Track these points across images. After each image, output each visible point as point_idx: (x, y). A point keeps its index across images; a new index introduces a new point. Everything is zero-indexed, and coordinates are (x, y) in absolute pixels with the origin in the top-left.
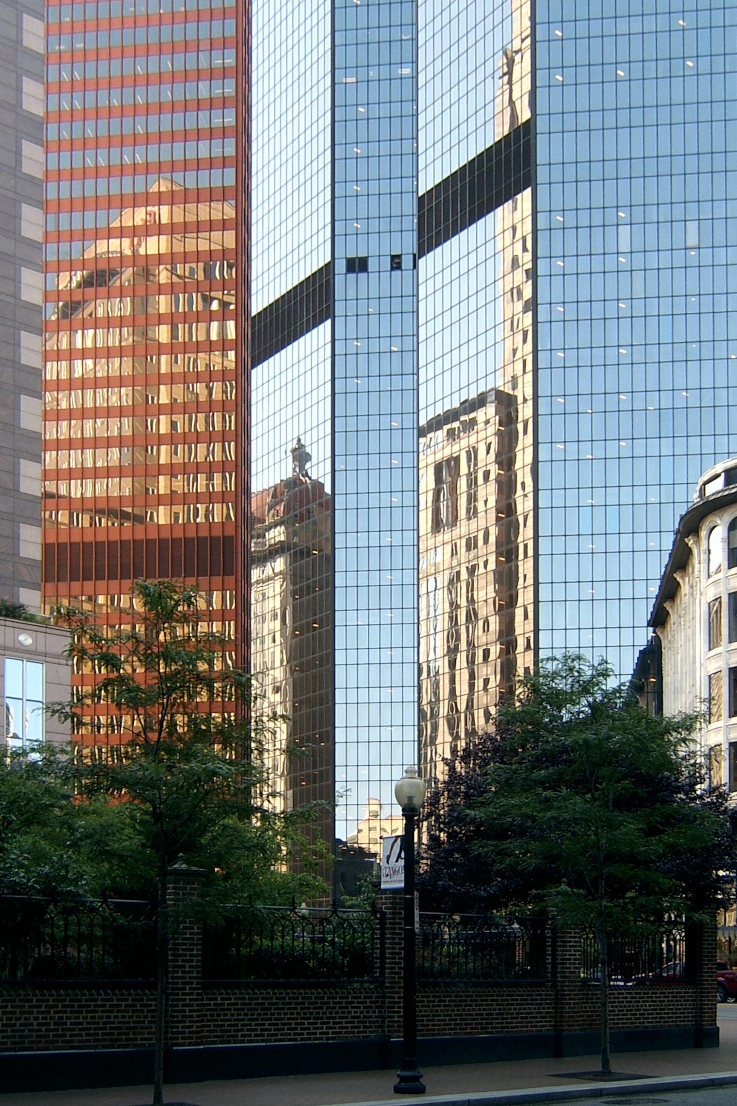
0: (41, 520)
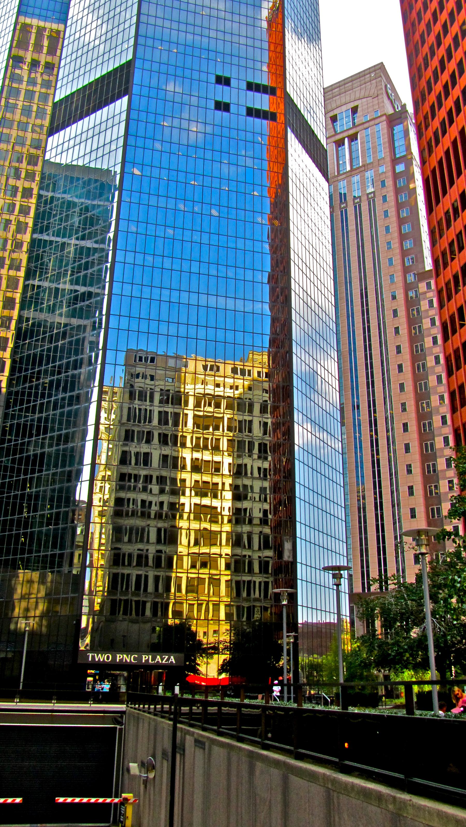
0: (198, 577)
